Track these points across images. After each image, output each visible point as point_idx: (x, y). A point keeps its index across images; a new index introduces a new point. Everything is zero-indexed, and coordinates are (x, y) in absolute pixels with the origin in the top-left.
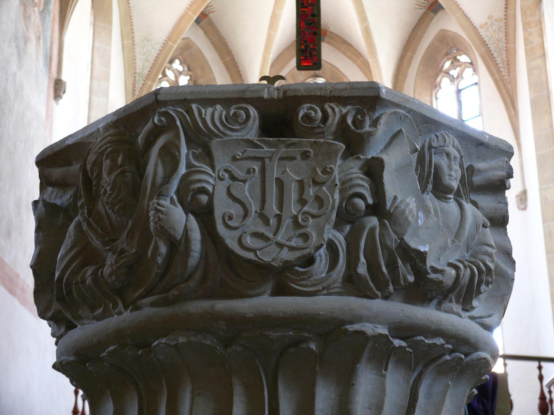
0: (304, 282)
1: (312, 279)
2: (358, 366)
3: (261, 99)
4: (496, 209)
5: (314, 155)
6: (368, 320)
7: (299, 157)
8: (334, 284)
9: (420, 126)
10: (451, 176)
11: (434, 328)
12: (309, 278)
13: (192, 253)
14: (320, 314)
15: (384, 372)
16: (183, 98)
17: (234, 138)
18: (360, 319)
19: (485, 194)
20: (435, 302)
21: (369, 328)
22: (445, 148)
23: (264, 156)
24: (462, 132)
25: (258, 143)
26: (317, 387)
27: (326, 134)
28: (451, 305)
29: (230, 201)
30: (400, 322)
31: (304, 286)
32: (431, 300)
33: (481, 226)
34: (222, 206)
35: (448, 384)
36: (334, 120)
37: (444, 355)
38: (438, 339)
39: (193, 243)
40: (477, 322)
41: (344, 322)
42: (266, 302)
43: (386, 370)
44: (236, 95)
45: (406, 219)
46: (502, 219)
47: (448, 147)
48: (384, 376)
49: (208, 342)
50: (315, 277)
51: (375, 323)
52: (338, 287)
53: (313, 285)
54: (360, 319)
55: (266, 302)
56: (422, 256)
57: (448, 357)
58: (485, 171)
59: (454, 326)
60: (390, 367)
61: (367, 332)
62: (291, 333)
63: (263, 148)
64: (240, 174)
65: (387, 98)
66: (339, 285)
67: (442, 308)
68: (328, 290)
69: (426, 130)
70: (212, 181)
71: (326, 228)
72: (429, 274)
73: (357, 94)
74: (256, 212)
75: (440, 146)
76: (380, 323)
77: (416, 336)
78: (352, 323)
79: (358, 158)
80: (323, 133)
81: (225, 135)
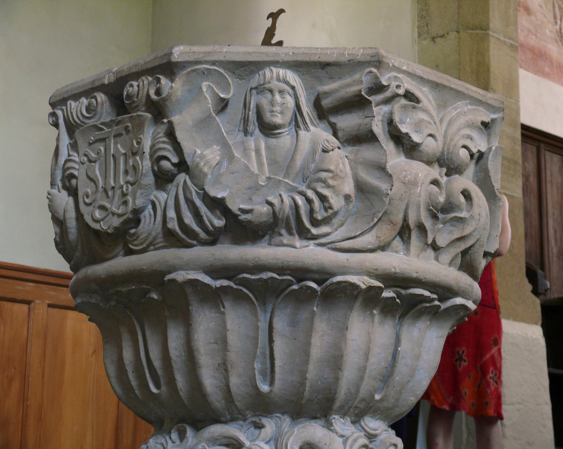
0: (136, 243)
1: (140, 238)
2: (191, 308)
3: (103, 85)
4: (360, 126)
5: (132, 128)
6: (182, 269)
7: (124, 133)
8: (155, 240)
9: (236, 72)
10: (273, 111)
11: (252, 265)
12: (138, 238)
13: (69, 230)
14: (143, 269)
15: (222, 309)
16: (61, 97)
17: (91, 124)
18: (173, 269)
19: (350, 112)
20: (267, 237)
21: (181, 276)
22: (265, 86)
23: (105, 137)
24: (293, 61)
25: (101, 126)
26: (168, 329)
27: (140, 107)
28: (281, 238)
29: (89, 181)
30: (211, 265)
31: (136, 245)
32: (263, 236)
33: (320, 150)
34: (85, 187)
35: (314, 311)
36: (143, 92)
37: (292, 285)
38: (265, 274)
39: (68, 222)
40: (329, 248)
41: (164, 274)
42: (120, 263)
43: (224, 307)
44: (90, 86)
45: (201, 171)
46: (370, 134)
47: (269, 83)
48: (223, 313)
49: (93, 301)
50: (142, 237)
51: (187, 270)
52: (161, 242)
53: (142, 244)
54: (173, 269)
55: (120, 263)
56: (223, 200)
57: (295, 287)
58: (337, 90)
59: (277, 259)
60: (227, 304)
61: (178, 280)
62: (134, 287)
63: (104, 130)
64: (93, 155)
65: (180, 60)
66: (161, 240)
67: (272, 243)
68: (154, 245)
69: (247, 72)
70: (77, 167)
71: (138, 194)
72: (239, 215)
73: (157, 64)
74: (102, 187)
75: (261, 85)
76: (193, 269)
77: (239, 274)
78: (170, 273)
79: (163, 123)
80: (137, 106)
81: (85, 123)
